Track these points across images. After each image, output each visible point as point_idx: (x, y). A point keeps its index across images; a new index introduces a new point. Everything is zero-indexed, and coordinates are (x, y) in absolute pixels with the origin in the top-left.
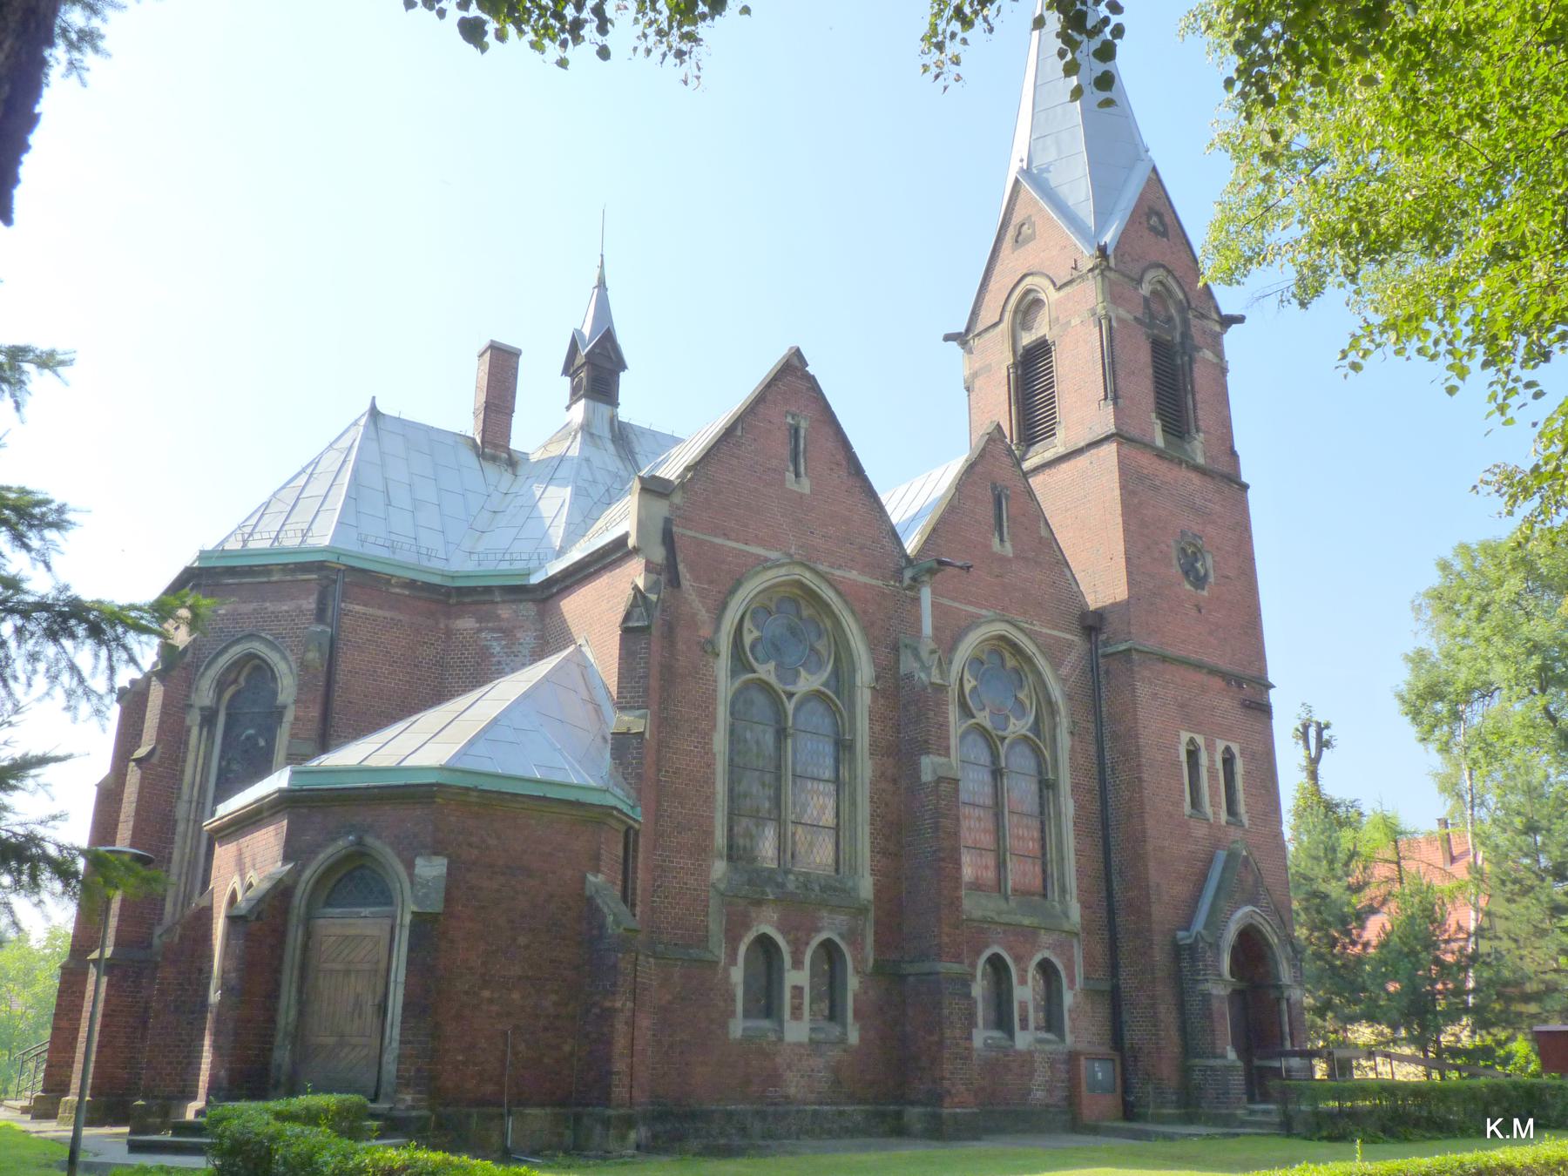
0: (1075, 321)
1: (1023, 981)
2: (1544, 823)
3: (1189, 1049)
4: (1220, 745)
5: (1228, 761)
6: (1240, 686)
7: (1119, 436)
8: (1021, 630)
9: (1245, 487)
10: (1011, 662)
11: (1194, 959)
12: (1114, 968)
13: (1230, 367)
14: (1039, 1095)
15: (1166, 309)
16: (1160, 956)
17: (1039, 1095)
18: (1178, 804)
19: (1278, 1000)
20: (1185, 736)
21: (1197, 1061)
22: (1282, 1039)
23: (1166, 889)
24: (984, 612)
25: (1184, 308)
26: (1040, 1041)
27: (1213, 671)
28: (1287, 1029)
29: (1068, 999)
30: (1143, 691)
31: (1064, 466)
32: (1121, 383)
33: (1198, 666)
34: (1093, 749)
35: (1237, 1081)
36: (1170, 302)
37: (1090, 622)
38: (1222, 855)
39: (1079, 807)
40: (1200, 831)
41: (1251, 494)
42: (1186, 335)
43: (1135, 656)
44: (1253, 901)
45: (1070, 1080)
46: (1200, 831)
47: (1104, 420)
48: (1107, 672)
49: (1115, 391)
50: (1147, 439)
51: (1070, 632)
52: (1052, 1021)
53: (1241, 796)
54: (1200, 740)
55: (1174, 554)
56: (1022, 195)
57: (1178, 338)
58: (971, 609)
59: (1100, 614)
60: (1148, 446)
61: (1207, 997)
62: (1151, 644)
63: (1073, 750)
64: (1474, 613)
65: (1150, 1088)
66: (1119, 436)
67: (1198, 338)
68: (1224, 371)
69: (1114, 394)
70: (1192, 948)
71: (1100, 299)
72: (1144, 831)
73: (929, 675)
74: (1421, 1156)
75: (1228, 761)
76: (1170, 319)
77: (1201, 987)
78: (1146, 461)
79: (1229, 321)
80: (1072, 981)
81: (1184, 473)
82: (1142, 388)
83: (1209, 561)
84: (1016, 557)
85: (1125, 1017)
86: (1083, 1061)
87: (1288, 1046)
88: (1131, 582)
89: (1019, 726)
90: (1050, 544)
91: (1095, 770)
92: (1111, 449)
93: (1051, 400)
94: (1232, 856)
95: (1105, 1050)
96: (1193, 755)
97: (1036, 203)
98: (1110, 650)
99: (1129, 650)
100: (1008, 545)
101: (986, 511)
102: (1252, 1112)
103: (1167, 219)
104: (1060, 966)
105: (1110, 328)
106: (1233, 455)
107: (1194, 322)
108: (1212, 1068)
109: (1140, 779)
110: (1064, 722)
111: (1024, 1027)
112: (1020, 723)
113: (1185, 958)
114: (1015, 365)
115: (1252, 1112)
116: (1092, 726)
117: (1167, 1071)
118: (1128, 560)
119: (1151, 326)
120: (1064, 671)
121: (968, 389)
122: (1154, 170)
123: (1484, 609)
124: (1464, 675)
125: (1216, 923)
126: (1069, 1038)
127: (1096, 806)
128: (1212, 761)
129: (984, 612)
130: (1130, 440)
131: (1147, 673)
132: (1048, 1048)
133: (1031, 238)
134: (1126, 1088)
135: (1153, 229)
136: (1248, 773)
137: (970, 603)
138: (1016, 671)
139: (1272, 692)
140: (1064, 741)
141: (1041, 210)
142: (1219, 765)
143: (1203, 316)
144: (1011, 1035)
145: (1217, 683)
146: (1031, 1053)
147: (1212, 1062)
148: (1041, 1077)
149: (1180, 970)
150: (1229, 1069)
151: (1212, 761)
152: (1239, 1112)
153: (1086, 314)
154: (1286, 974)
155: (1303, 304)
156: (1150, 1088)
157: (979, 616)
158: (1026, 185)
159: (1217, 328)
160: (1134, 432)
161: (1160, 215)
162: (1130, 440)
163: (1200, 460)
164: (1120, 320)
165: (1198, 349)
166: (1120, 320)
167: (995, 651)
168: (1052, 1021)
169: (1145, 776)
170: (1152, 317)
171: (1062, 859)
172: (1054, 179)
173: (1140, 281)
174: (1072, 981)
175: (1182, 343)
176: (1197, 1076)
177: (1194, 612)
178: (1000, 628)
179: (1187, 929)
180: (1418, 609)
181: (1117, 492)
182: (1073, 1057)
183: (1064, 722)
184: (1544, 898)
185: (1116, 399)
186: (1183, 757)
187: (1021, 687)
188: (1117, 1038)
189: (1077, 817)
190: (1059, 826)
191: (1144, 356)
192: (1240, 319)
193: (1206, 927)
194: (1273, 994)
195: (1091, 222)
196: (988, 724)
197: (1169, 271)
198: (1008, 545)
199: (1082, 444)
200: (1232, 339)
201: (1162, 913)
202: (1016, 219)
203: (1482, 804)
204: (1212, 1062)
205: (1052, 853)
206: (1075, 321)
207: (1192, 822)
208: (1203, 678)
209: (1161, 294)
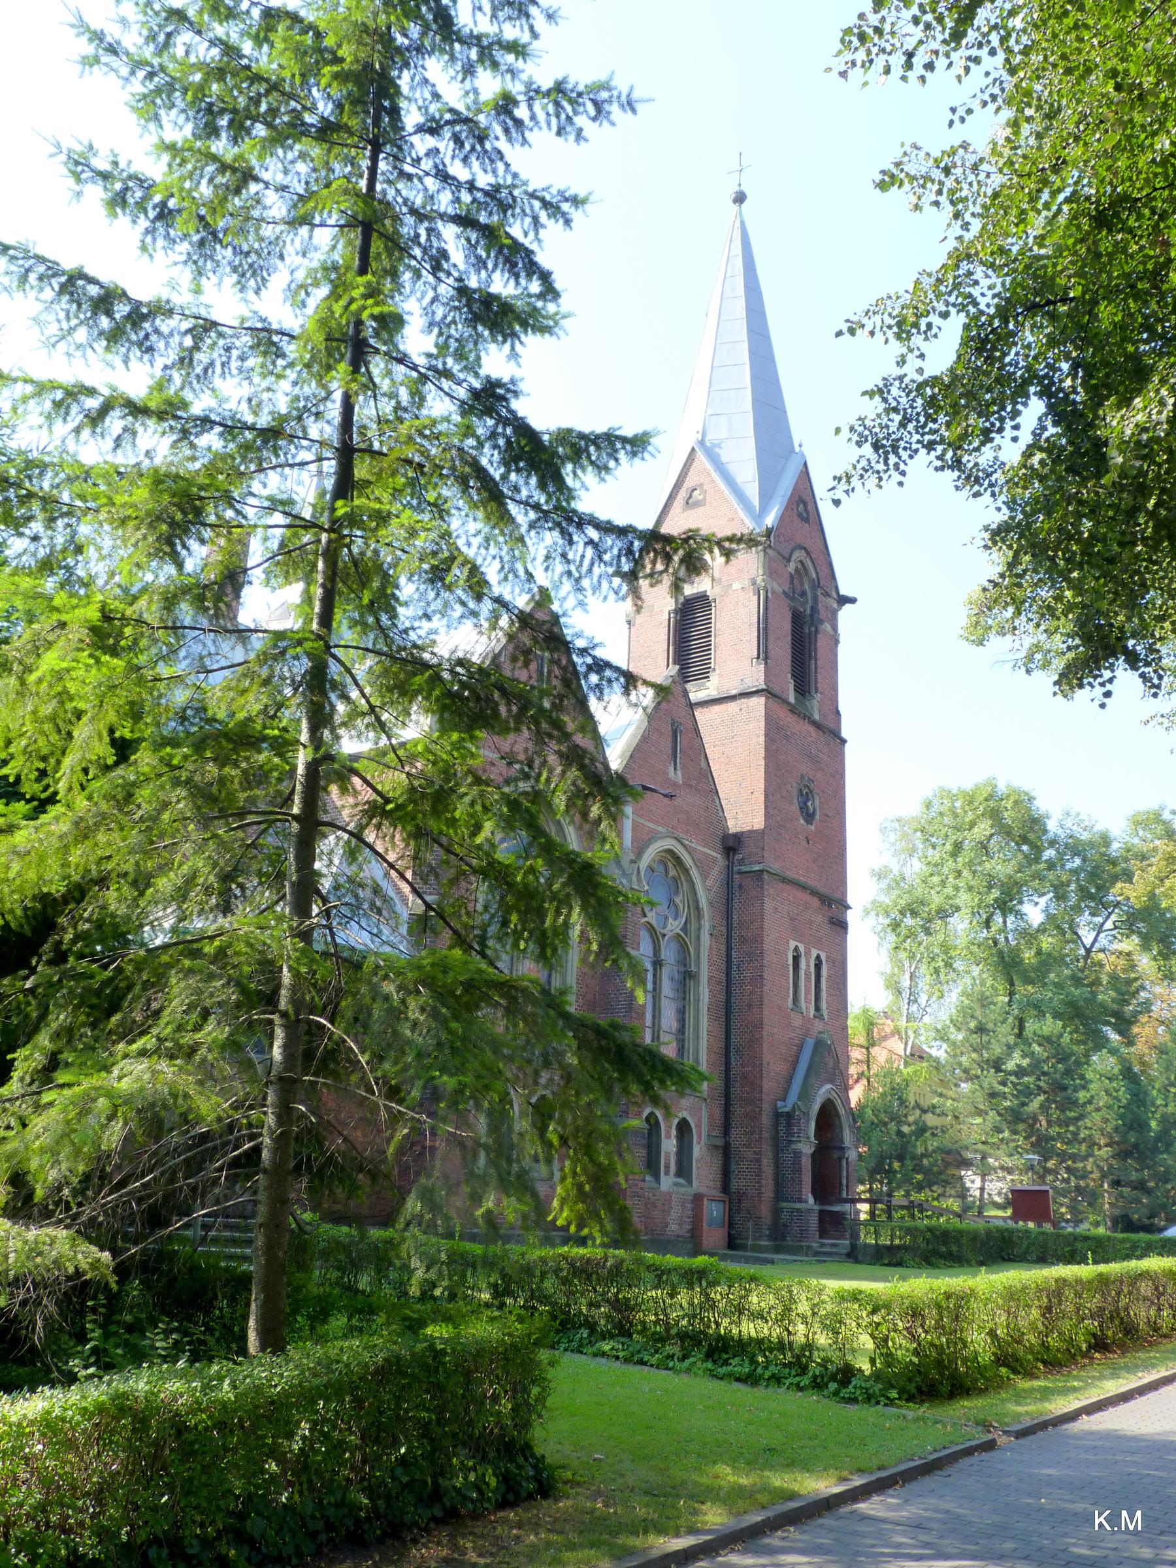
0: (736, 586)
1: (668, 1137)
2: (990, 1026)
3: (780, 1193)
4: (814, 953)
5: (818, 966)
6: (830, 906)
7: (767, 692)
8: (685, 846)
9: (844, 741)
10: (673, 873)
11: (789, 1125)
12: (726, 1128)
13: (841, 639)
14: (673, 1228)
15: (802, 585)
16: (766, 1120)
17: (673, 1228)
18: (785, 999)
19: (840, 1159)
20: (793, 944)
21: (784, 1204)
22: (840, 1190)
23: (773, 1066)
24: (660, 829)
25: (816, 585)
26: (676, 1184)
27: (814, 893)
28: (844, 1182)
29: (697, 1151)
30: (769, 905)
31: (716, 708)
32: (770, 647)
33: (803, 887)
34: (723, 948)
35: (814, 1220)
36: (805, 579)
37: (731, 843)
38: (810, 1042)
39: (712, 995)
40: (797, 1021)
41: (848, 748)
42: (814, 609)
43: (765, 876)
44: (832, 1081)
45: (694, 1216)
46: (797, 1021)
47: (755, 676)
48: (740, 886)
49: (766, 653)
50: (784, 696)
51: (713, 849)
52: (684, 1170)
53: (824, 995)
54: (802, 948)
55: (795, 793)
56: (696, 464)
57: (808, 612)
58: (651, 825)
59: (738, 837)
60: (785, 701)
61: (798, 1155)
62: (775, 867)
63: (711, 949)
64: (948, 847)
65: (750, 1224)
66: (767, 692)
67: (823, 614)
68: (837, 642)
69: (764, 654)
70: (789, 1116)
71: (761, 572)
72: (761, 1020)
73: (630, 881)
74: (951, 1276)
75: (818, 966)
76: (803, 594)
77: (794, 1146)
78: (783, 714)
79: (845, 600)
80: (700, 1137)
81: (806, 727)
82: (783, 650)
83: (817, 802)
84: (685, 784)
85: (733, 1167)
86: (706, 1202)
87: (844, 1195)
88: (767, 815)
89: (674, 926)
90: (706, 774)
91: (724, 967)
92: (759, 702)
93: (707, 647)
94: (819, 1044)
95: (717, 1193)
96: (796, 959)
97: (709, 474)
98: (744, 869)
99: (762, 871)
100: (679, 772)
101: (667, 743)
102: (823, 1245)
103: (810, 507)
104: (693, 1126)
105: (767, 598)
106: (838, 713)
107: (821, 598)
108: (798, 1210)
109: (761, 977)
110: (706, 925)
111: (667, 1173)
112: (675, 923)
113: (785, 1121)
114: (676, 611)
115: (823, 1245)
116: (724, 930)
117: (765, 1210)
118: (766, 796)
119: (792, 599)
120: (710, 882)
121: (629, 623)
122: (805, 465)
123: (958, 847)
124: (936, 900)
125: (806, 1094)
126: (695, 1182)
127: (723, 997)
128: (808, 966)
129: (660, 829)
130: (774, 695)
131: (771, 891)
132: (682, 1190)
133: (697, 504)
134: (731, 1225)
135: (800, 515)
136: (830, 977)
137: (651, 821)
138: (674, 879)
139: (849, 912)
140: (706, 939)
141: (713, 481)
142: (812, 969)
143: (827, 594)
144: (657, 1178)
145: (815, 902)
146: (670, 1194)
147: (798, 1206)
148: (675, 1213)
149: (777, 1132)
150: (809, 1211)
151: (808, 966)
152: (815, 1245)
153: (747, 583)
154: (848, 1138)
155: (1028, 672)
156: (750, 1224)
157: (658, 832)
158: (700, 455)
159: (835, 605)
160: (776, 690)
161: (805, 504)
162: (774, 695)
163: (817, 717)
164: (773, 592)
165: (821, 622)
166: (773, 592)
167: (663, 862)
168: (684, 1170)
169: (765, 975)
170: (794, 590)
171: (697, 1037)
172: (725, 456)
173: (789, 560)
174: (700, 1137)
175: (812, 615)
176: (785, 1217)
177: (804, 843)
178: (669, 843)
179: (784, 1100)
180: (883, 830)
181: (762, 739)
182: (698, 1198)
183: (706, 925)
184: (986, 1085)
185: (766, 658)
186: (790, 961)
187: (677, 892)
188: (725, 1187)
189: (710, 1003)
190: (697, 1010)
191: (787, 626)
192: (852, 601)
193: (799, 1098)
194: (836, 1154)
195: (756, 502)
196: (654, 923)
197: (808, 553)
198: (679, 772)
199: (734, 692)
200: (845, 615)
201: (770, 1085)
202: (689, 483)
203: (916, 1001)
204: (798, 1206)
205: (689, 1032)
206: (736, 586)
207: (793, 1014)
208: (806, 897)
209: (802, 571)
